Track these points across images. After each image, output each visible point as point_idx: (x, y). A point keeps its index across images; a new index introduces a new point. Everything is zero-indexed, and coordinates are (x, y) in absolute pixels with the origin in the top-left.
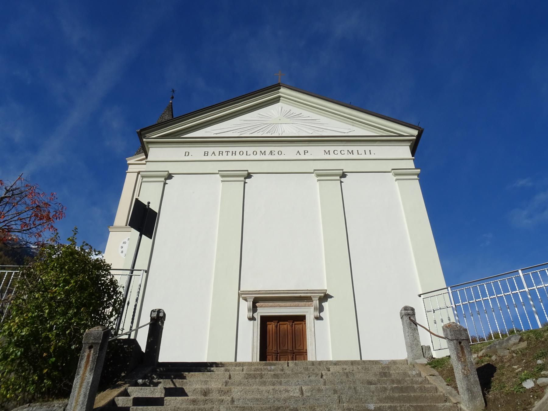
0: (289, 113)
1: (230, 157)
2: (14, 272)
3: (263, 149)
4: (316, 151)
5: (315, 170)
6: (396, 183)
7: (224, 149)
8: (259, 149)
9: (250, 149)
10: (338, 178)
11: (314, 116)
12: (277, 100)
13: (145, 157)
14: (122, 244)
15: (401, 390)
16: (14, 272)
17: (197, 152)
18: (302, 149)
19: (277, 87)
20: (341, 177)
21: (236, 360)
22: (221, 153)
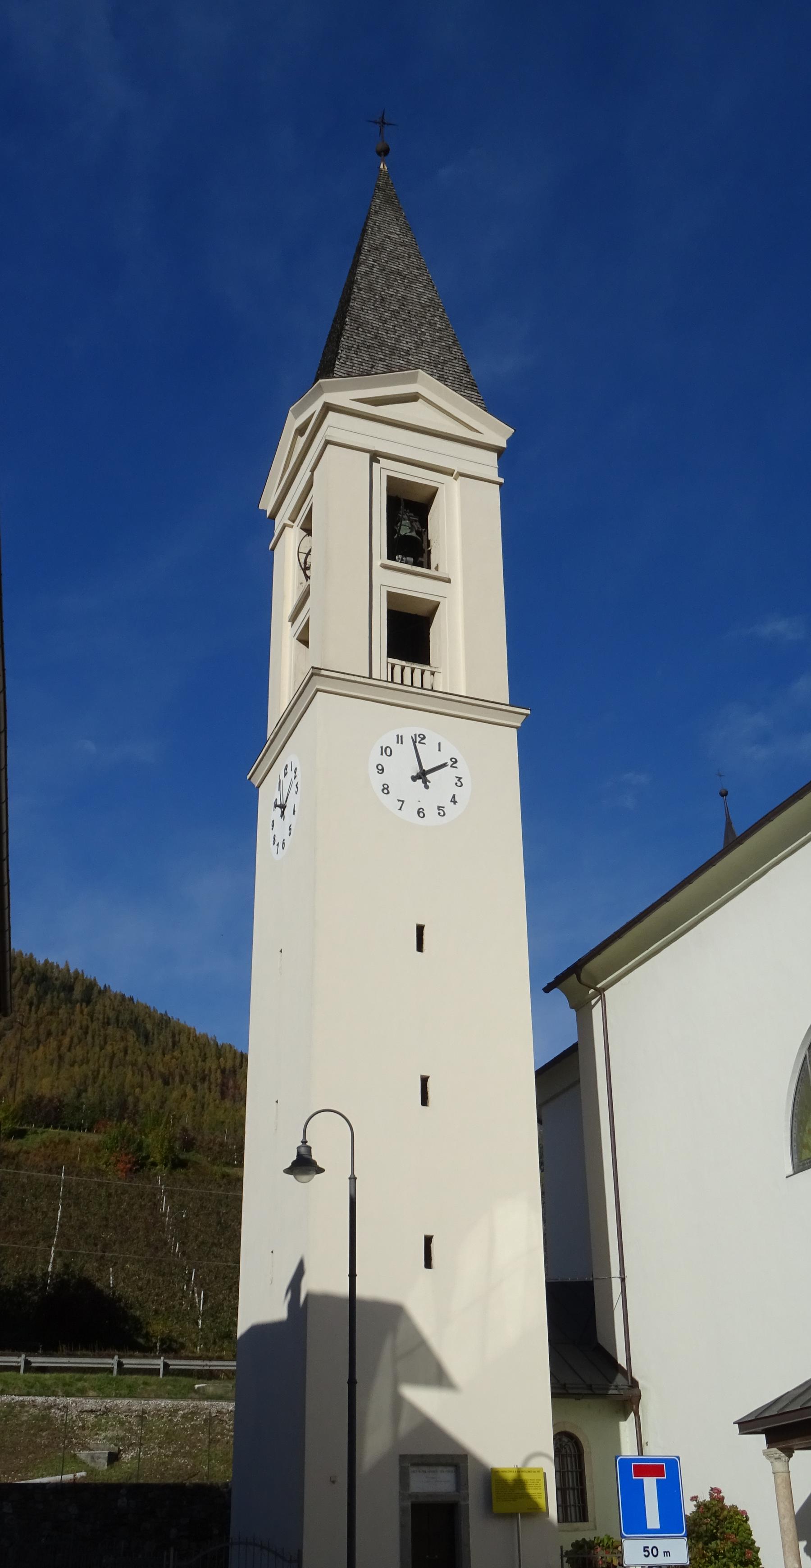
14: (378, 781)
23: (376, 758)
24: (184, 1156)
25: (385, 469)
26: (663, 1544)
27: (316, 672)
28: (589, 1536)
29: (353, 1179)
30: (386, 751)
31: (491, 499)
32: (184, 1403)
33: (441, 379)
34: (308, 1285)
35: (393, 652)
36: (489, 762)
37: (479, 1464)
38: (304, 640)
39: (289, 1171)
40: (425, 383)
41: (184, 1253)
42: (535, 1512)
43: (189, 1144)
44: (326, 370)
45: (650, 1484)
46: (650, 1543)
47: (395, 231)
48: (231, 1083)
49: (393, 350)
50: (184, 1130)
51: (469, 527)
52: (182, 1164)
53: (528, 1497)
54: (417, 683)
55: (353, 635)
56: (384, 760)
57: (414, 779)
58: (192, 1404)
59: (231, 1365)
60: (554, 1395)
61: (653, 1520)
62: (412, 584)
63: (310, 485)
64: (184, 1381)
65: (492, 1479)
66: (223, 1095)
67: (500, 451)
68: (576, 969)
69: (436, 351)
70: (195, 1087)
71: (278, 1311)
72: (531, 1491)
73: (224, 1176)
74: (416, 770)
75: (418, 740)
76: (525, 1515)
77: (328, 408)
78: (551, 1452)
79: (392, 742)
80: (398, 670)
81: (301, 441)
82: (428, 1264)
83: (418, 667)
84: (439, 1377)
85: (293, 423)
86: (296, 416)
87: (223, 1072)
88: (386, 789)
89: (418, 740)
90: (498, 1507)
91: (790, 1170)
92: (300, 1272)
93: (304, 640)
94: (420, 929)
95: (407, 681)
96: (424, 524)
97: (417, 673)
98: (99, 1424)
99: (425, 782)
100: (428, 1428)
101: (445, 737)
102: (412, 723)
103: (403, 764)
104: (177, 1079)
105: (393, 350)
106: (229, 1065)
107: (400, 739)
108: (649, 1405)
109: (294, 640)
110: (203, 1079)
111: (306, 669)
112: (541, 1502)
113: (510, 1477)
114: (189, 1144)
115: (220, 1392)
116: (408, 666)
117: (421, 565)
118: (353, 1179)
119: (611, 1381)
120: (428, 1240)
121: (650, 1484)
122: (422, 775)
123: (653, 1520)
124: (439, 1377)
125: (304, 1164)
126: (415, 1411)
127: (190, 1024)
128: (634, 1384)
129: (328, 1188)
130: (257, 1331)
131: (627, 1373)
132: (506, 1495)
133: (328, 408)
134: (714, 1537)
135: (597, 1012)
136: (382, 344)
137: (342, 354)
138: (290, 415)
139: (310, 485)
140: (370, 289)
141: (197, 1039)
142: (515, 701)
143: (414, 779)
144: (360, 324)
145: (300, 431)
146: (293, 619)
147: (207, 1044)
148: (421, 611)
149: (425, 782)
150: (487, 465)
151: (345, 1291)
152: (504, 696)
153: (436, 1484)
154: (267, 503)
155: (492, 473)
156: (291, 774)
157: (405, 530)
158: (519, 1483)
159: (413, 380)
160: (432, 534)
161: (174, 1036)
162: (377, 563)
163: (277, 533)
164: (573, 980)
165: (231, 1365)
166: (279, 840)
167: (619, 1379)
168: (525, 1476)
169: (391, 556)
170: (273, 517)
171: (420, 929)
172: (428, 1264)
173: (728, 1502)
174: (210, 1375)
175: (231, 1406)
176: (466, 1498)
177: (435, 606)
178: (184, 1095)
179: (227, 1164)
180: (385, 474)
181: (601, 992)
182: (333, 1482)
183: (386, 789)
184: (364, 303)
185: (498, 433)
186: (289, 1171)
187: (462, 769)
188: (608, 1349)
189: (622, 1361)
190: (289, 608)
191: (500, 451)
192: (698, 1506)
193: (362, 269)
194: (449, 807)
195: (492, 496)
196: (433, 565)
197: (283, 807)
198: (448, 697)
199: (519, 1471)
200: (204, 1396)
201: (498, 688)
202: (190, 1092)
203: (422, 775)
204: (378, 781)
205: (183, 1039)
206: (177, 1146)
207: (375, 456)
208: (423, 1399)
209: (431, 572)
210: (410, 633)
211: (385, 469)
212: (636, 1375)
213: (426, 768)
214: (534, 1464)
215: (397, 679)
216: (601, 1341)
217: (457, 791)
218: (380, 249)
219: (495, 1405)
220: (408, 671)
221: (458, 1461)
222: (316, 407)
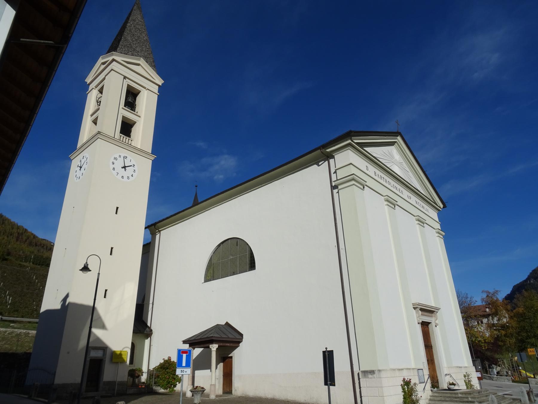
12: (392, 144)
14: (112, 166)
19: (395, 134)
23: (112, 160)
24: (7, 257)
25: (127, 82)
26: (185, 370)
27: (99, 133)
28: (134, 368)
29: (99, 274)
30: (115, 159)
31: (154, 98)
32: (9, 330)
33: (147, 62)
34: (69, 300)
35: (121, 133)
36: (143, 168)
37: (110, 349)
38: (95, 122)
39: (81, 270)
40: (142, 62)
41: (4, 286)
42: (124, 362)
43: (9, 254)
44: (113, 48)
45: (184, 356)
46: (182, 369)
47: (139, 17)
48: (20, 237)
49: (134, 50)
50: (8, 250)
51: (147, 104)
52: (6, 260)
53: (122, 358)
54: (127, 142)
55: (111, 124)
56: (115, 161)
57: (122, 168)
58: (12, 330)
59: (37, 320)
60: (134, 332)
61: (184, 364)
62: (129, 115)
63: (104, 79)
64: (7, 323)
65: (113, 353)
66: (17, 240)
67: (159, 86)
68: (154, 224)
69: (146, 54)
70: (8, 237)
71: (58, 306)
72: (123, 357)
73: (20, 264)
74: (123, 166)
75: (125, 157)
76: (121, 363)
77: (114, 60)
78: (130, 347)
79: (118, 157)
80: (122, 137)
81: (103, 67)
82: (105, 297)
83: (128, 138)
84: (103, 327)
85: (101, 60)
86: (103, 59)
87: (18, 233)
88: (114, 169)
89: (125, 157)
90: (114, 360)
91: (203, 281)
92: (67, 296)
93: (95, 122)
94: (117, 208)
95: (124, 141)
96: (135, 100)
97: (127, 139)
98: (14, 335)
99: (125, 169)
100: (98, 340)
101: (132, 158)
102: (124, 153)
103: (120, 163)
104: (2, 233)
105: (134, 50)
106: (21, 232)
107: (120, 156)
108: (154, 336)
109: (91, 122)
110: (11, 235)
111: (95, 132)
112: (125, 359)
113: (118, 353)
114: (9, 254)
115: (19, 327)
116: (125, 137)
117: (132, 110)
118: (99, 274)
119: (145, 329)
120: (106, 290)
121: (184, 356)
122: (125, 167)
123: (184, 364)
124: (103, 327)
125: (86, 269)
126: (95, 335)
127: (9, 218)
128: (151, 330)
129: (91, 276)
130: (48, 312)
131: (150, 328)
132: (117, 358)
133: (114, 60)
134: (168, 369)
135: (157, 237)
136: (131, 47)
137: (120, 46)
138: (100, 58)
139: (104, 79)
140: (130, 31)
141: (11, 223)
142: (153, 153)
143: (122, 168)
144: (126, 40)
145: (103, 63)
146: (92, 115)
147: (14, 224)
148: (131, 123)
149: (125, 169)
150: (156, 89)
151: (92, 305)
152: (150, 150)
153: (98, 354)
154: (88, 80)
155: (157, 92)
156: (85, 159)
157: (130, 100)
158: (120, 355)
159: (139, 60)
160: (137, 103)
161: (3, 220)
162: (121, 107)
163: (89, 90)
164: (153, 227)
165: (37, 320)
166: (78, 176)
167: (147, 329)
168: (122, 353)
169: (125, 106)
170: (89, 84)
171: (117, 208)
172: (105, 297)
173: (172, 360)
174: (13, 322)
175: (34, 332)
176: (105, 358)
177: (135, 123)
178: (4, 239)
179: (21, 261)
180: (127, 83)
181: (160, 231)
182: (68, 353)
183: (114, 169)
184: (128, 34)
185: (160, 82)
186: (81, 270)
187: (136, 168)
188: (146, 322)
189: (149, 324)
190: (91, 112)
191: (159, 86)
192: (165, 361)
193: (129, 24)
194: (130, 177)
195: (155, 98)
196: (136, 111)
197: (81, 167)
198: (135, 148)
199: (121, 351)
200: (13, 327)
201: (149, 148)
202: (6, 238)
203: (125, 167)
204: (112, 166)
205: (6, 222)
206: (5, 254)
207: (125, 78)
208: (97, 332)
209: (135, 113)
210: (127, 128)
211: (127, 82)
212: (152, 328)
213: (126, 165)
214: (125, 350)
215: (121, 140)
216: (144, 319)
217: (133, 173)
218: (134, 20)
219: (115, 333)
220: (125, 138)
221: (104, 348)
222: (110, 59)
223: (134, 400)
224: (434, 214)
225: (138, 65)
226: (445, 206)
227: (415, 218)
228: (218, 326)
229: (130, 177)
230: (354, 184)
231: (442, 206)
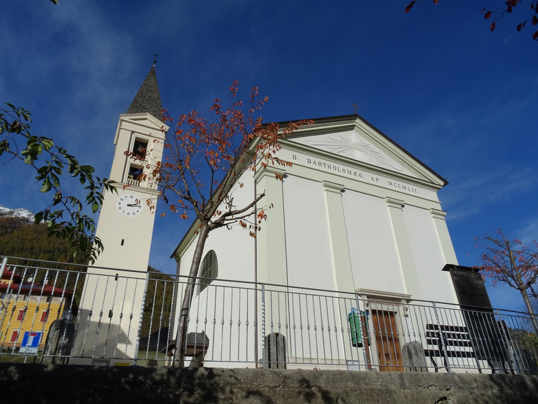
0: (357, 141)
1: (326, 169)
2: (26, 268)
3: (350, 169)
4: (384, 181)
5: (387, 197)
6: (388, 208)
7: (323, 161)
8: (347, 168)
9: (341, 166)
10: (339, 191)
11: (378, 150)
12: (351, 128)
13: (443, 185)
14: (118, 206)
15: (398, 355)
16: (26, 268)
17: (302, 158)
18: (375, 176)
19: (353, 117)
20: (341, 191)
21: (146, 272)
22: (320, 164)
25: (134, 136)
40: (148, 116)
56: (121, 202)
88: (120, 208)
101: (143, 197)
107: (126, 197)
159: (146, 115)
183: (120, 208)
191: (166, 133)
194: (136, 213)
223: (335, 371)
224: (433, 195)
225: (146, 119)
226: (446, 183)
227: (384, 200)
228: (140, 331)
229: (136, 213)
230: (265, 175)
231: (442, 183)
